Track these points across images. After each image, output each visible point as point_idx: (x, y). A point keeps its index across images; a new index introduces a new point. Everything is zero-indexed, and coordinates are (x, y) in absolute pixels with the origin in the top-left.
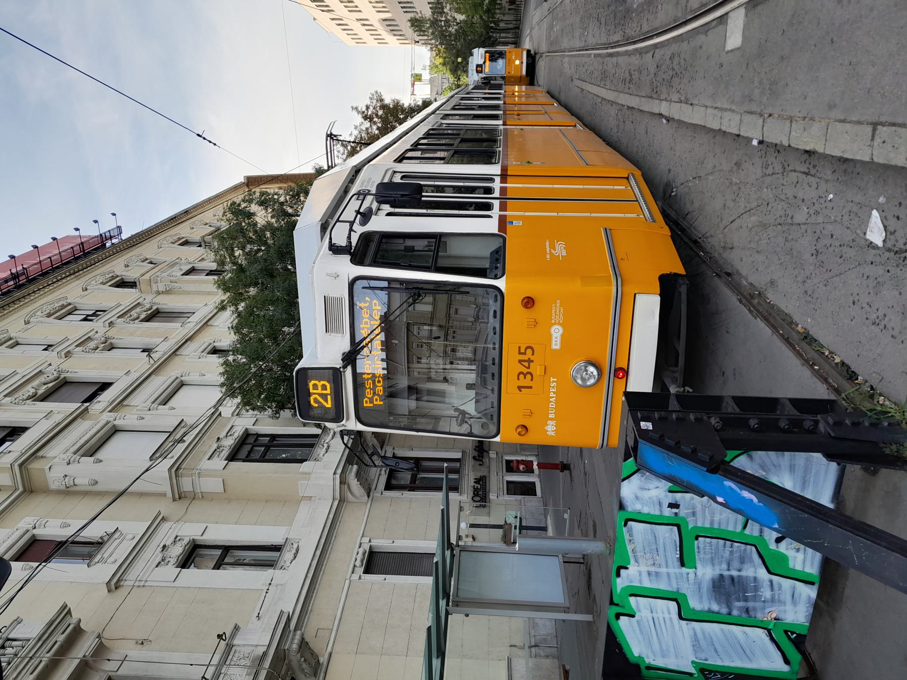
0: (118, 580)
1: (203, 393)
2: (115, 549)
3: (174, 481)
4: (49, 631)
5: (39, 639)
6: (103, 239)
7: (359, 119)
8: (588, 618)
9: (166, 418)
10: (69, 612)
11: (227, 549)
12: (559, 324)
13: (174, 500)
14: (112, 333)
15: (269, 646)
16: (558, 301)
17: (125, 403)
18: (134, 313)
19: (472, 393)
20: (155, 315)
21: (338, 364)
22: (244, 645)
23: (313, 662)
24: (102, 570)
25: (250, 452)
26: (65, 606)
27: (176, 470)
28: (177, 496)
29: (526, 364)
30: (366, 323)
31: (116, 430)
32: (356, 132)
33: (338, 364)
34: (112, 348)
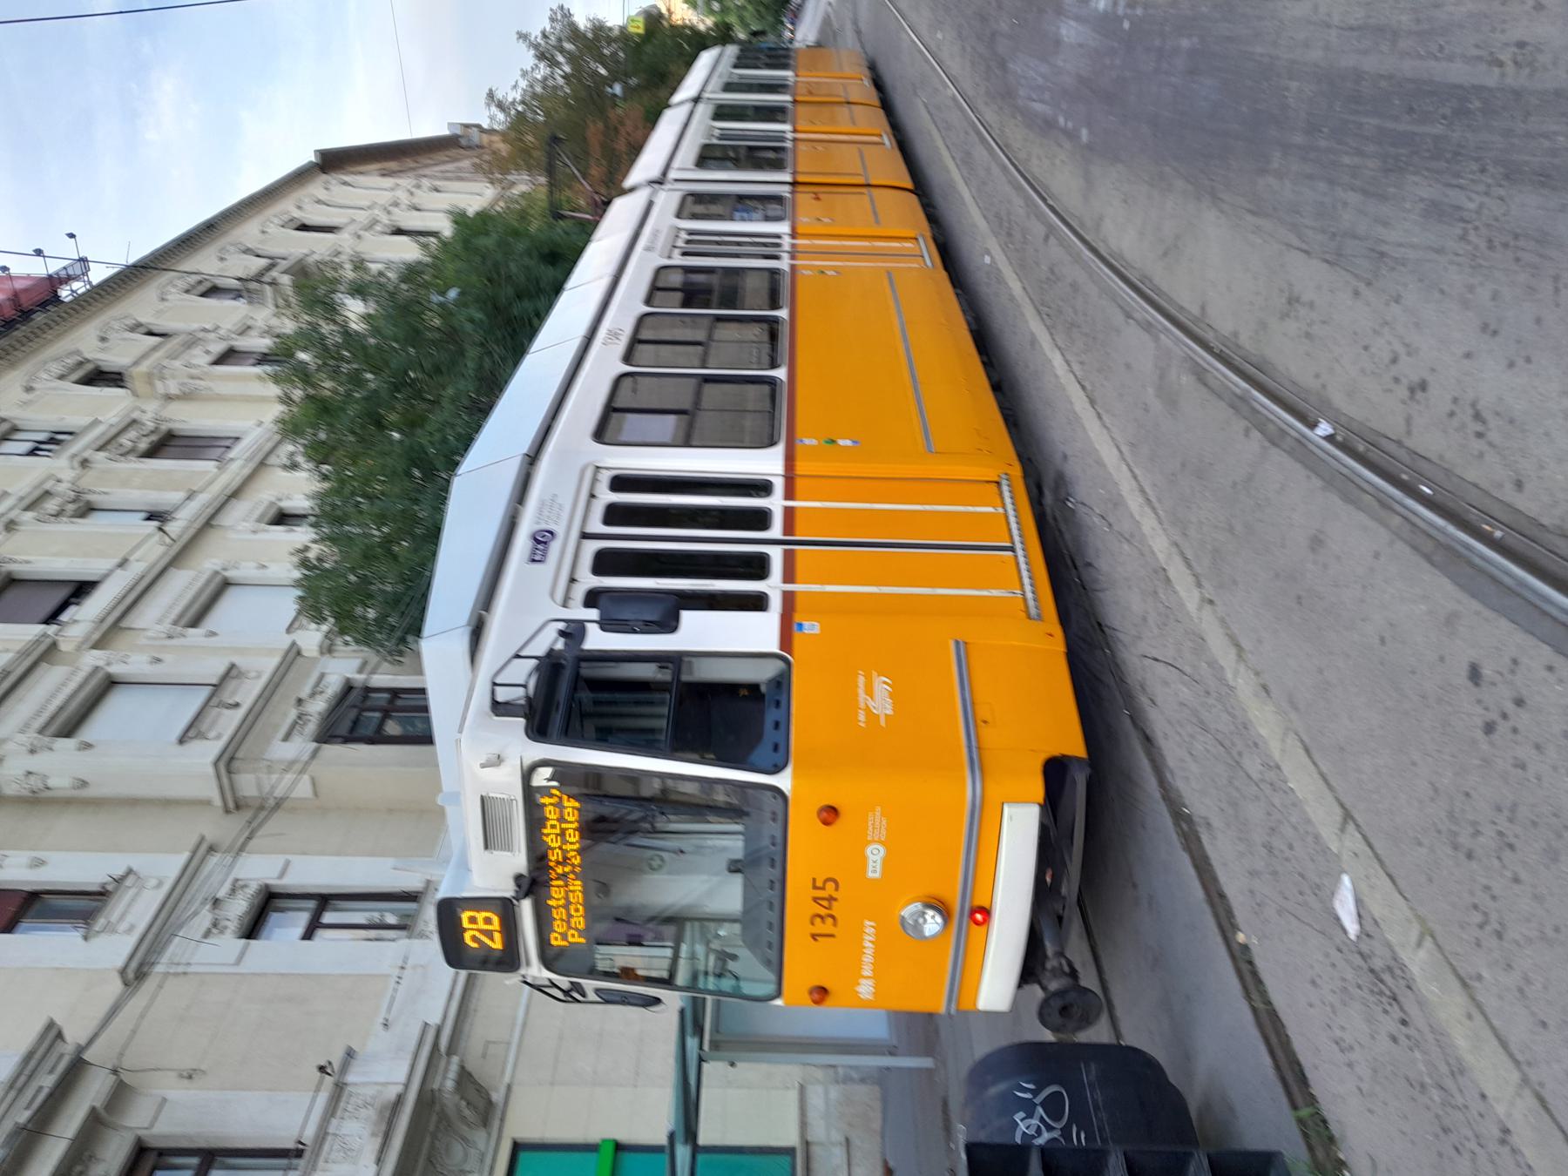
0: (141, 965)
1: (265, 623)
2: (129, 905)
3: (225, 781)
4: (27, 1072)
5: (11, 1087)
6: (54, 282)
7: (528, 58)
8: (926, 1062)
9: (200, 658)
10: (60, 1036)
11: (325, 901)
12: (880, 842)
13: (227, 811)
14: (88, 480)
15: (407, 1086)
16: (878, 809)
17: (124, 624)
18: (125, 440)
19: (737, 881)
20: (165, 444)
21: (507, 890)
22: (365, 1084)
23: (481, 1104)
24: (111, 948)
25: (356, 722)
26: (51, 1025)
27: (228, 762)
28: (231, 805)
29: (825, 903)
30: (553, 827)
31: (111, 684)
32: (523, 84)
33: (507, 890)
34: (87, 510)
